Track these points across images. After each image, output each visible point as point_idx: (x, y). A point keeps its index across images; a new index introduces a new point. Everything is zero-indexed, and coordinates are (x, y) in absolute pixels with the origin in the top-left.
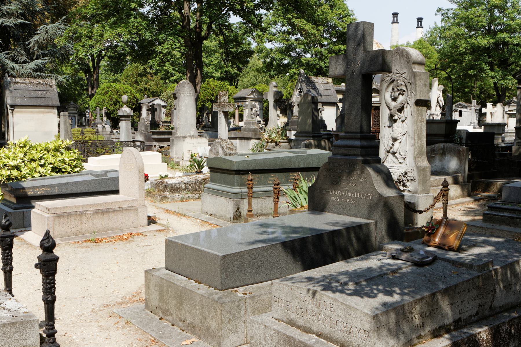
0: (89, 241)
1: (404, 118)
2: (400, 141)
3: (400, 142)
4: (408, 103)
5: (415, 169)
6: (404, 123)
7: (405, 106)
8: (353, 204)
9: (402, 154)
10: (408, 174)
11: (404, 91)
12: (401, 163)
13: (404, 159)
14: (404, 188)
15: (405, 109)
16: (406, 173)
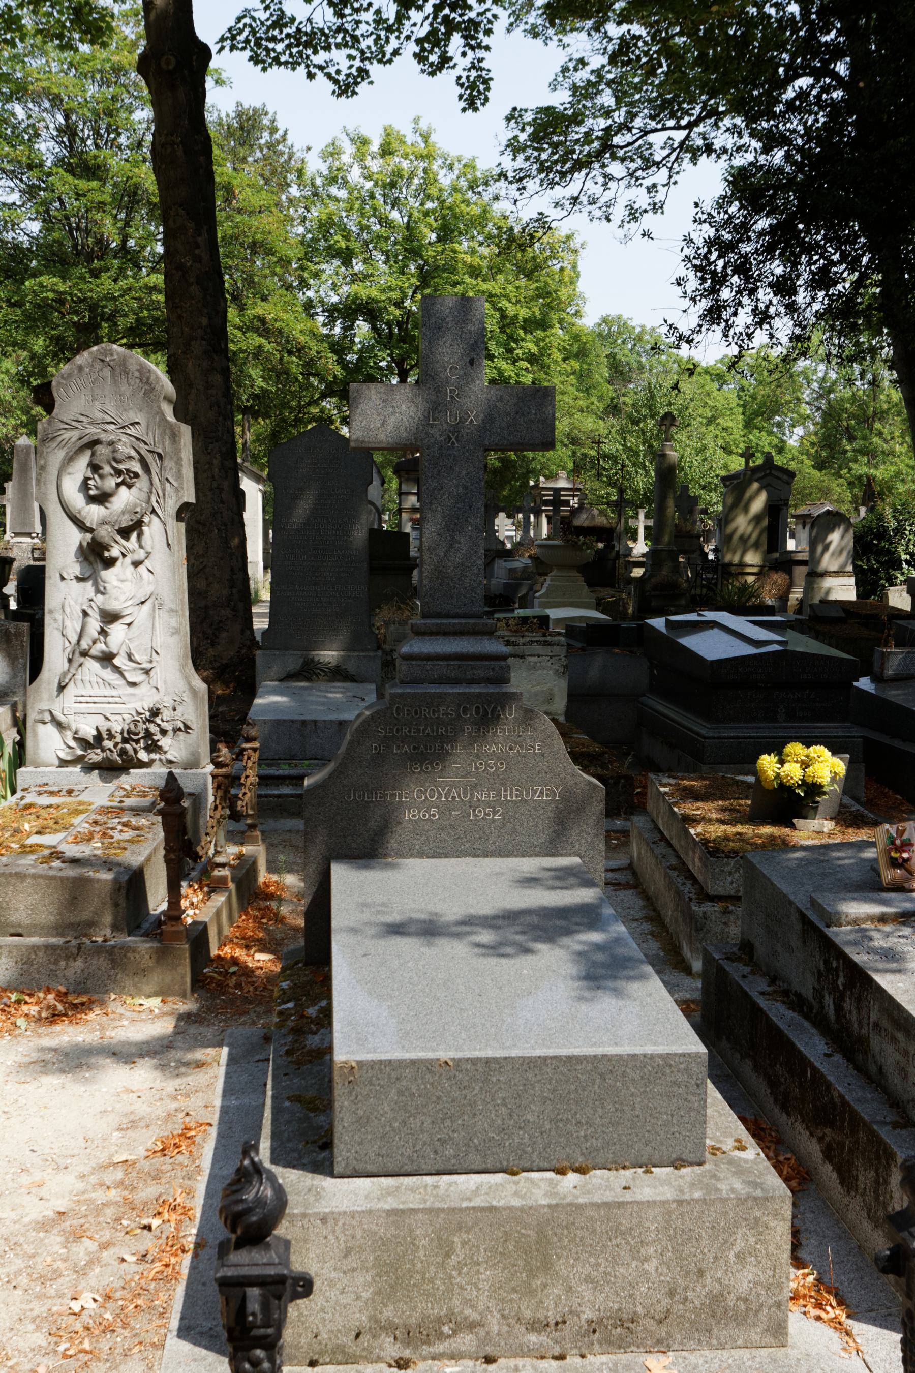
1: (141, 554)
2: (127, 620)
3: (129, 625)
4: (153, 511)
5: (187, 697)
6: (142, 568)
7: (146, 519)
8: (494, 821)
9: (137, 657)
10: (166, 714)
11: (136, 475)
12: (133, 684)
13: (147, 672)
14: (154, 756)
15: (145, 529)
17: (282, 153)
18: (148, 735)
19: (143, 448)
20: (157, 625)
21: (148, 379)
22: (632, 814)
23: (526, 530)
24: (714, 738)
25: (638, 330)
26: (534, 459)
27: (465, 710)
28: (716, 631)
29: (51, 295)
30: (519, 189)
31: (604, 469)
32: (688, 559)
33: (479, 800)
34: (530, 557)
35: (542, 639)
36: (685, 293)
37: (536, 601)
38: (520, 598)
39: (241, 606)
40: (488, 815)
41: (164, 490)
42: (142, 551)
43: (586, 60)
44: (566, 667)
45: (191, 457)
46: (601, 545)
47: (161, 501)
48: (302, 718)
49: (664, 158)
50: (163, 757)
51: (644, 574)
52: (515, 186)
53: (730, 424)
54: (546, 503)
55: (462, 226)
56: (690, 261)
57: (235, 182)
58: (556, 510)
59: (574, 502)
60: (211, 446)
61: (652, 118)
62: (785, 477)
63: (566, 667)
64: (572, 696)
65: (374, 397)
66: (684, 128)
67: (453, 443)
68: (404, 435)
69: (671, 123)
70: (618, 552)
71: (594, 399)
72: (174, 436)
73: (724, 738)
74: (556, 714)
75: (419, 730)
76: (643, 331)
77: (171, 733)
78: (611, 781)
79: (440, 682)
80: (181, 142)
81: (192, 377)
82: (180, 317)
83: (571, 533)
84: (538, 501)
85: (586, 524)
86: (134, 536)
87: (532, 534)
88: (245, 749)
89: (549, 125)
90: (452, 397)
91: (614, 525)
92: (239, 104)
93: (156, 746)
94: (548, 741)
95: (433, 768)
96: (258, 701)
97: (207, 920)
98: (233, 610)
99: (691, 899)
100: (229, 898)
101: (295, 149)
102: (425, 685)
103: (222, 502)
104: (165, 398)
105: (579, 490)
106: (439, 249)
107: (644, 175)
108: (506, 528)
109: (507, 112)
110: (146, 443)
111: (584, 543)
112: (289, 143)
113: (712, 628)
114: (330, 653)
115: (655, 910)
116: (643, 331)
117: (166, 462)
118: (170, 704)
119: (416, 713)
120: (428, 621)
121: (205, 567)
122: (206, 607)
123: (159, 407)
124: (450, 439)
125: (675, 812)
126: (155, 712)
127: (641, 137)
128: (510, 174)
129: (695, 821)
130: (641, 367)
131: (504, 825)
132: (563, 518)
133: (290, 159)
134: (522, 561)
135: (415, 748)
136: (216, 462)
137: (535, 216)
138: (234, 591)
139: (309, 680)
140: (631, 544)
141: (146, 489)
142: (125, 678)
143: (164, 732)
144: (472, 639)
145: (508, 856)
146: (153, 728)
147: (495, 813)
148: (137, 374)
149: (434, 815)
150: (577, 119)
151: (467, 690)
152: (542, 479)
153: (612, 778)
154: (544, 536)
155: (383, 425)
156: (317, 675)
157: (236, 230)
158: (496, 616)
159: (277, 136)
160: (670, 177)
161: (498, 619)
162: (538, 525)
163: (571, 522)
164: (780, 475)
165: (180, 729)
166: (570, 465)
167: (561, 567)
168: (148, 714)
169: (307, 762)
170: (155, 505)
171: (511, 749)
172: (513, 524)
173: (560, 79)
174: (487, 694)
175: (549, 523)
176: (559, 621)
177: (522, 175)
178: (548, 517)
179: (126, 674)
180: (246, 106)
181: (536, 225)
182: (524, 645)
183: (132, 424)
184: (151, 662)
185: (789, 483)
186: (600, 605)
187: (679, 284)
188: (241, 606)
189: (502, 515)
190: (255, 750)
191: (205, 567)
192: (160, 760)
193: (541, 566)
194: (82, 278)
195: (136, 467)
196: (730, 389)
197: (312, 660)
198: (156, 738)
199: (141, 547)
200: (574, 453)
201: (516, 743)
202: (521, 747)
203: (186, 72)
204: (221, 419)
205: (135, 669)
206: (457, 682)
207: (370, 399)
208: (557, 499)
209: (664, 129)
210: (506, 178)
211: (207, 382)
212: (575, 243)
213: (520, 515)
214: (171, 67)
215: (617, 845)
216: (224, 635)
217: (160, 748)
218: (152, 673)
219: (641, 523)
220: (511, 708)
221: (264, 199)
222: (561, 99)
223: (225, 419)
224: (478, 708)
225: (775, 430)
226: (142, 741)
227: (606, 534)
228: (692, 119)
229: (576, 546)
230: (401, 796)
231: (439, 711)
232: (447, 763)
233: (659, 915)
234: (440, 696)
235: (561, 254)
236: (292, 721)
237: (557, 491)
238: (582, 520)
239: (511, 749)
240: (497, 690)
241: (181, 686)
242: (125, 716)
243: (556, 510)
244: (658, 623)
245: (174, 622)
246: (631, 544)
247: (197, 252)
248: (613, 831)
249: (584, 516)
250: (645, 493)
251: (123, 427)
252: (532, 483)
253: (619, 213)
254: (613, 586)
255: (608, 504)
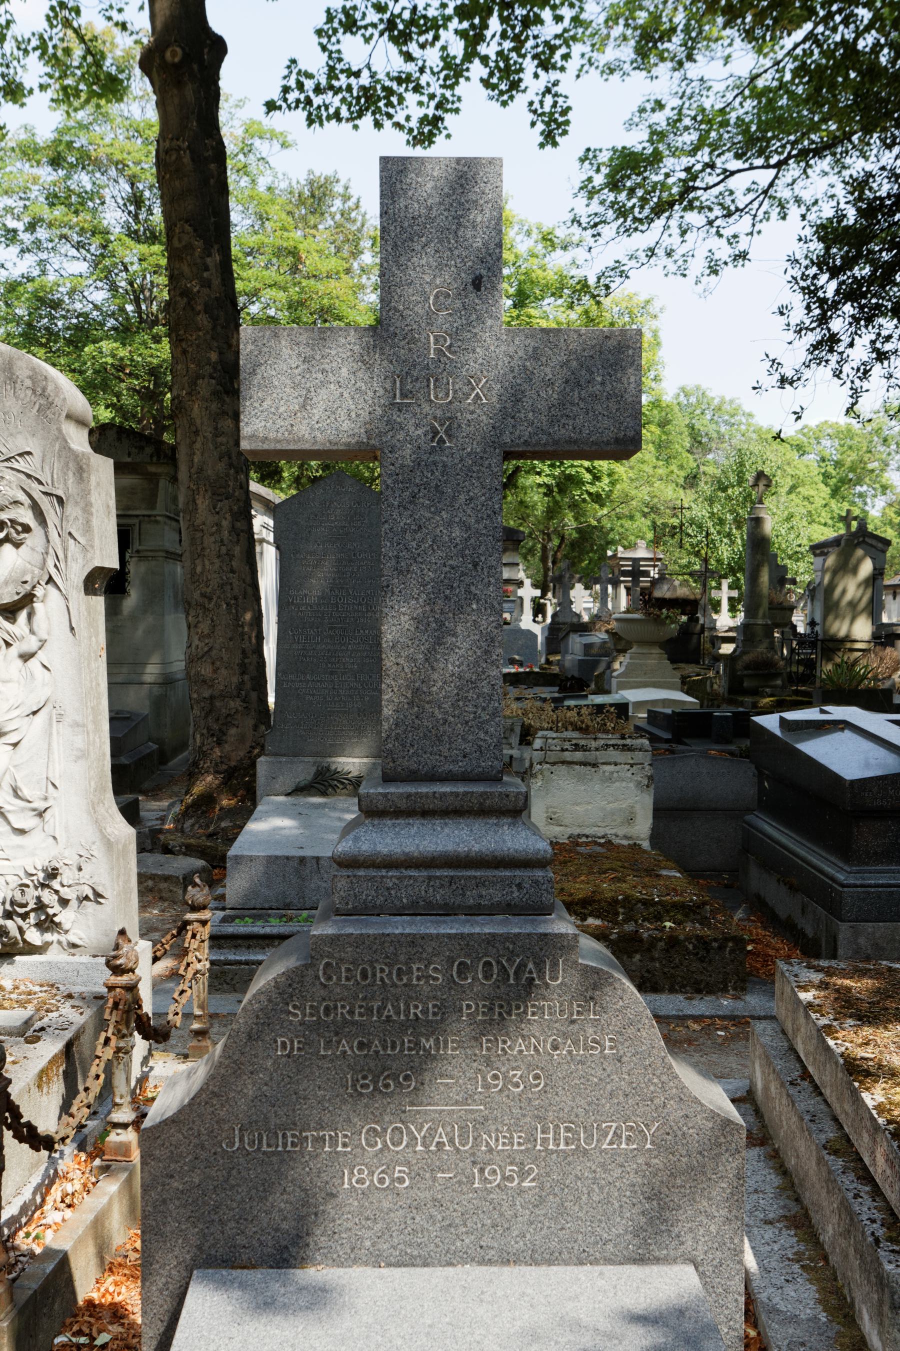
0: (633, 750)
1: (31, 644)
2: (12, 738)
3: (15, 745)
4: (50, 580)
5: (98, 850)
6: (33, 663)
7: (39, 592)
8: (521, 1191)
9: (26, 792)
10: (67, 876)
11: (27, 529)
12: (22, 832)
13: (41, 814)
14: (48, 937)
15: (37, 606)
16: (53, 874)
17: (354, 221)
18: (41, 906)
19: (36, 490)
20: (55, 745)
21: (44, 389)
22: (743, 989)
23: (604, 602)
24: (856, 886)
25: (716, 402)
26: (612, 529)
27: (463, 969)
28: (847, 734)
29: (109, 360)
30: (594, 236)
31: (689, 535)
32: (782, 633)
33: (490, 1150)
34: (607, 631)
35: (621, 742)
36: (788, 325)
37: (614, 682)
38: (597, 676)
39: (254, 695)
40: (510, 1179)
41: (65, 550)
42: (33, 638)
43: (663, 102)
44: (650, 778)
45: (112, 503)
46: (684, 618)
47: (62, 566)
48: (301, 853)
49: (747, 206)
50: (63, 938)
51: (735, 650)
52: (590, 232)
53: (812, 493)
54: (625, 573)
55: (538, 292)
56: (797, 283)
57: (301, 247)
58: (636, 581)
59: (654, 573)
60: (219, 505)
61: (738, 156)
62: (880, 545)
63: (650, 778)
64: (659, 812)
65: (286, 352)
66: (774, 167)
67: (441, 441)
68: (346, 425)
69: (760, 162)
70: (703, 625)
71: (674, 467)
72: (82, 471)
73: (870, 886)
74: (638, 838)
75: (370, 1010)
76: (723, 401)
77: (74, 903)
78: (715, 945)
79: (414, 910)
80: (189, 147)
81: (198, 422)
82: (184, 352)
83: (653, 606)
84: (616, 572)
85: (668, 595)
86: (23, 616)
87: (610, 606)
88: (188, 923)
89: (627, 166)
90: (439, 352)
91: (699, 597)
92: (311, 172)
93: (52, 922)
94: (631, 1031)
95: (399, 1085)
96: (254, 826)
97: (65, 1245)
98: (244, 701)
99: (877, 1241)
100: (129, 1181)
101: (367, 217)
102: (384, 918)
103: (232, 571)
104: (69, 417)
105: (660, 559)
106: (514, 314)
107: (725, 224)
108: (582, 601)
109: (581, 153)
110: (40, 483)
111: (667, 617)
112: (362, 210)
113: (842, 730)
114: (350, 760)
115: (798, 1200)
116: (723, 401)
117: (70, 509)
118: (73, 860)
119: (364, 976)
120: (392, 789)
121: (211, 649)
122: (212, 698)
123: (59, 430)
124: (435, 433)
125: (828, 1048)
126: (53, 874)
127: (722, 181)
128: (584, 220)
129: (868, 1073)
130: (721, 437)
131: (542, 1200)
132: (642, 589)
133: (363, 226)
134: (599, 636)
135: (361, 1046)
136: (225, 523)
137: (612, 264)
138: (246, 678)
139: (324, 794)
140: (715, 616)
141: (40, 549)
142: (9, 823)
143: (64, 902)
144: (478, 825)
145: (550, 1263)
146: (48, 897)
147: (523, 1175)
148: (28, 383)
149: (401, 1180)
150: (656, 158)
151: (467, 930)
152: (620, 549)
153: (715, 940)
154: (623, 609)
155: (304, 406)
156: (334, 788)
157: (303, 296)
158: (568, 703)
159: (351, 203)
160: (754, 225)
161: (569, 708)
162: (616, 597)
163: (650, 594)
164: (874, 542)
165: (87, 898)
166: (650, 535)
167: (642, 643)
168: (41, 875)
169: (305, 913)
170: (53, 572)
171: (555, 1048)
172: (590, 595)
173: (636, 119)
174: (507, 937)
175: (628, 594)
176: (639, 705)
177: (597, 220)
178: (628, 589)
179: (10, 817)
180: (317, 174)
181: (612, 273)
182: (597, 749)
183: (20, 455)
184: (46, 799)
185: (884, 552)
186: (688, 686)
187: (782, 314)
188: (254, 695)
189: (579, 587)
190: (204, 923)
191: (211, 649)
192: (59, 942)
193: (619, 643)
194: (144, 343)
195: (26, 516)
196: (811, 458)
197: (328, 769)
198: (51, 911)
199: (32, 632)
200: (654, 523)
201: (565, 1036)
202: (576, 1043)
203: (195, 67)
204: (232, 471)
205: (23, 810)
206: (447, 911)
207: (278, 356)
208: (636, 572)
209: (752, 168)
210: (580, 224)
211: (216, 429)
212: (654, 308)
213: (598, 587)
214: (177, 60)
215: (725, 1039)
216: (233, 731)
217: (58, 925)
218: (47, 815)
219: (724, 594)
220: (555, 965)
221: (334, 263)
222: (636, 140)
223: (237, 472)
224: (488, 964)
225: (857, 500)
226: (32, 915)
227: (689, 606)
228: (782, 158)
229: (658, 620)
230: (334, 1141)
231: (410, 971)
232: (427, 1076)
233: (807, 1215)
234: (413, 941)
235: (640, 319)
236: (287, 858)
237: (636, 561)
238: (664, 592)
239: (555, 1048)
240: (528, 929)
241: (89, 834)
242: (10, 878)
243: (636, 581)
244: (770, 722)
245: (79, 741)
246: (715, 616)
247: (205, 275)
248: (719, 1017)
249: (666, 587)
250: (729, 564)
251: (8, 460)
252: (609, 553)
253: (698, 266)
254: (698, 663)
255: (691, 574)
